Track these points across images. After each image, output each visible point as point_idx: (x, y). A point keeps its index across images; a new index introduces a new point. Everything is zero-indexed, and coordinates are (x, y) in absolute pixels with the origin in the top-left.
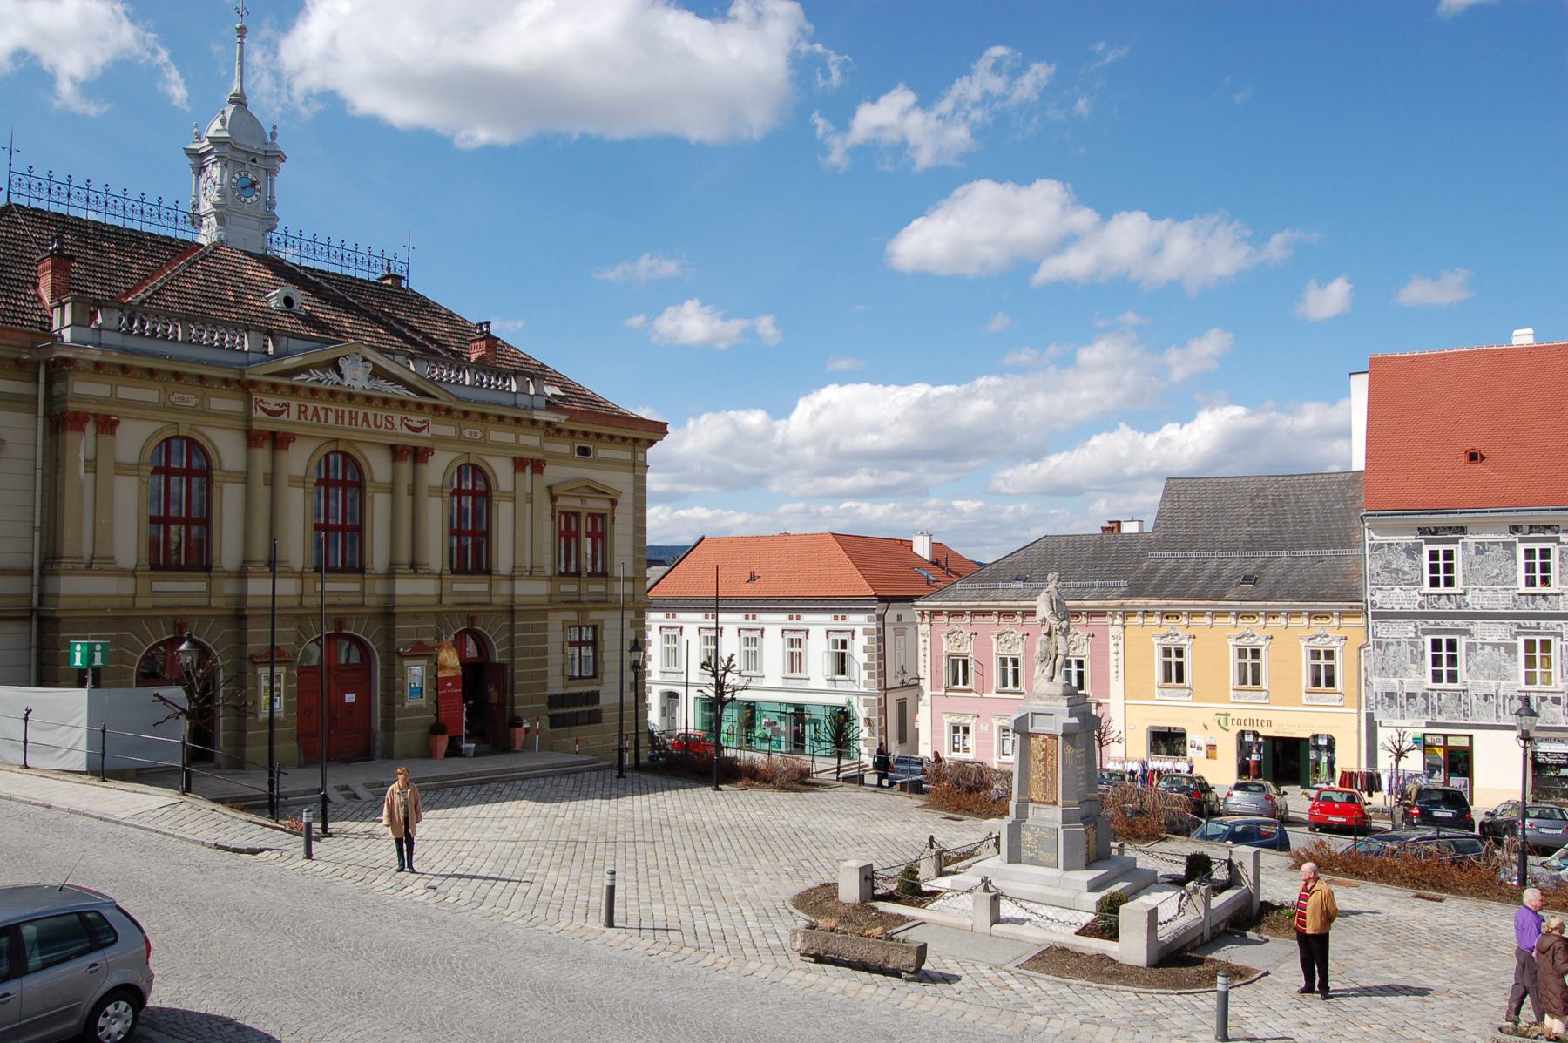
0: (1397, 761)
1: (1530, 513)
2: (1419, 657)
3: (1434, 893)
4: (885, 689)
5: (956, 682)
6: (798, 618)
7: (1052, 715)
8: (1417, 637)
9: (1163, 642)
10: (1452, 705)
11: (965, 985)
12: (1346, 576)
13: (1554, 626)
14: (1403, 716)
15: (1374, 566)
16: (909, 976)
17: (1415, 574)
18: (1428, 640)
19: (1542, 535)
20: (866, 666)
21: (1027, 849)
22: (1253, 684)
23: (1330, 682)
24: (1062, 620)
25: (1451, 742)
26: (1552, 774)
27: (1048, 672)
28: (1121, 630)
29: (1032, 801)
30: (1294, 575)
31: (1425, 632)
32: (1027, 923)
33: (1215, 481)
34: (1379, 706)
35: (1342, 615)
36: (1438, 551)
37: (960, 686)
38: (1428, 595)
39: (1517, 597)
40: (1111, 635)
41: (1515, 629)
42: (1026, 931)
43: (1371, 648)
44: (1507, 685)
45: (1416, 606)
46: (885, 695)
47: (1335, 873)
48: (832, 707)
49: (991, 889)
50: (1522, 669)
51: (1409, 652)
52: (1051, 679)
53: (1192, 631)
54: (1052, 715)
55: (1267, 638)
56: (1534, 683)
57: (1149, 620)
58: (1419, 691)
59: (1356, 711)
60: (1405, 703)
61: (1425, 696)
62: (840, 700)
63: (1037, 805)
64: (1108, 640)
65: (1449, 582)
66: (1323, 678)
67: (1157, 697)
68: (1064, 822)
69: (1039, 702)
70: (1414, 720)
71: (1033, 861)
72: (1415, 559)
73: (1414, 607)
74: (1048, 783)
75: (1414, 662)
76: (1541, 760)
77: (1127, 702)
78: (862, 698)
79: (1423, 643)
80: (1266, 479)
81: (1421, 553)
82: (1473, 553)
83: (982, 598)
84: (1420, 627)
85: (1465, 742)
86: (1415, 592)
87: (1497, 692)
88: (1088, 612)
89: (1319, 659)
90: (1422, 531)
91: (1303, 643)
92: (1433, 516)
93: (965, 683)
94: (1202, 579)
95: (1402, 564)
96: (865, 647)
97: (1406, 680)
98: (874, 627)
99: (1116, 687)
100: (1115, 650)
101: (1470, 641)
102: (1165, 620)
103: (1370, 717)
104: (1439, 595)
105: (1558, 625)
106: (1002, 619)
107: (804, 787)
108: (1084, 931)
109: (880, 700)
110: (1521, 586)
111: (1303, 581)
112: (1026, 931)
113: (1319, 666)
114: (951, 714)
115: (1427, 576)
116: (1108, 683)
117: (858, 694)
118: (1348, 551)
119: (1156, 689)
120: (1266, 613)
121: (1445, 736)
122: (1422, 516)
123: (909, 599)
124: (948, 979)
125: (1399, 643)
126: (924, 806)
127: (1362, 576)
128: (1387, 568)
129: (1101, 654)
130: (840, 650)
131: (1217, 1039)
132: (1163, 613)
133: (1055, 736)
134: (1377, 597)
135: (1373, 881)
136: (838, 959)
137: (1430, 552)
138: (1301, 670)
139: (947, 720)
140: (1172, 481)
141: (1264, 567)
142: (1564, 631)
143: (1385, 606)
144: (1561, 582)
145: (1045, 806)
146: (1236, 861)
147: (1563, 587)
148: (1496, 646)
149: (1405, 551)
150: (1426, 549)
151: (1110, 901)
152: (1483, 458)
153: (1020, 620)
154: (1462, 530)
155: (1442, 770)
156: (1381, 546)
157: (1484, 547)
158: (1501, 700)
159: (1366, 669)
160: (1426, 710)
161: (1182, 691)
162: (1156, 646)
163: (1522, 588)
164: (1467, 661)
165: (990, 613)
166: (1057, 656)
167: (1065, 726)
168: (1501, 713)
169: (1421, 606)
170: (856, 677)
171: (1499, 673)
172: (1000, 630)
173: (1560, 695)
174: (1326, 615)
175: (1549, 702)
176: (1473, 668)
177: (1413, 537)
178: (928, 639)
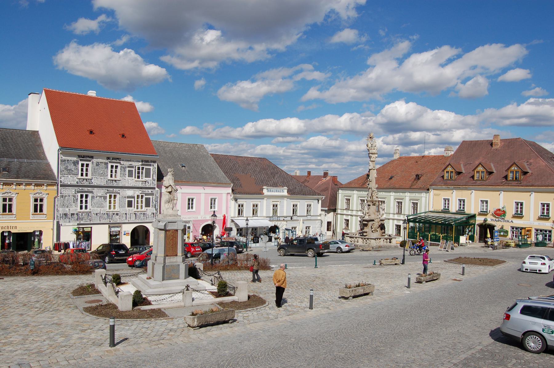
8: (76, 194)
10: (86, 217)
14: (69, 222)
17: (76, 171)
18: (79, 195)
19: (116, 161)
25: (86, 230)
26: (114, 238)
31: (78, 192)
34: (61, 219)
35: (48, 185)
38: (80, 179)
43: (59, 197)
44: (103, 210)
45: (76, 183)
59: (52, 221)
60: (70, 217)
61: (77, 214)
63: (169, 257)
66: (38, 208)
72: (76, 166)
73: (75, 183)
76: (112, 234)
84: (76, 190)
85: (89, 230)
90: (79, 156)
91: (31, 196)
95: (71, 167)
103: (58, 223)
104: (84, 179)
118: (41, 161)
121: (83, 228)
128: (66, 169)
133: (177, 230)
138: (30, 206)
148: (101, 197)
154: (92, 157)
156: (65, 160)
158: (101, 215)
159: (57, 205)
160: (78, 219)
163: (109, 178)
168: (101, 219)
169: (77, 183)
176: (93, 204)
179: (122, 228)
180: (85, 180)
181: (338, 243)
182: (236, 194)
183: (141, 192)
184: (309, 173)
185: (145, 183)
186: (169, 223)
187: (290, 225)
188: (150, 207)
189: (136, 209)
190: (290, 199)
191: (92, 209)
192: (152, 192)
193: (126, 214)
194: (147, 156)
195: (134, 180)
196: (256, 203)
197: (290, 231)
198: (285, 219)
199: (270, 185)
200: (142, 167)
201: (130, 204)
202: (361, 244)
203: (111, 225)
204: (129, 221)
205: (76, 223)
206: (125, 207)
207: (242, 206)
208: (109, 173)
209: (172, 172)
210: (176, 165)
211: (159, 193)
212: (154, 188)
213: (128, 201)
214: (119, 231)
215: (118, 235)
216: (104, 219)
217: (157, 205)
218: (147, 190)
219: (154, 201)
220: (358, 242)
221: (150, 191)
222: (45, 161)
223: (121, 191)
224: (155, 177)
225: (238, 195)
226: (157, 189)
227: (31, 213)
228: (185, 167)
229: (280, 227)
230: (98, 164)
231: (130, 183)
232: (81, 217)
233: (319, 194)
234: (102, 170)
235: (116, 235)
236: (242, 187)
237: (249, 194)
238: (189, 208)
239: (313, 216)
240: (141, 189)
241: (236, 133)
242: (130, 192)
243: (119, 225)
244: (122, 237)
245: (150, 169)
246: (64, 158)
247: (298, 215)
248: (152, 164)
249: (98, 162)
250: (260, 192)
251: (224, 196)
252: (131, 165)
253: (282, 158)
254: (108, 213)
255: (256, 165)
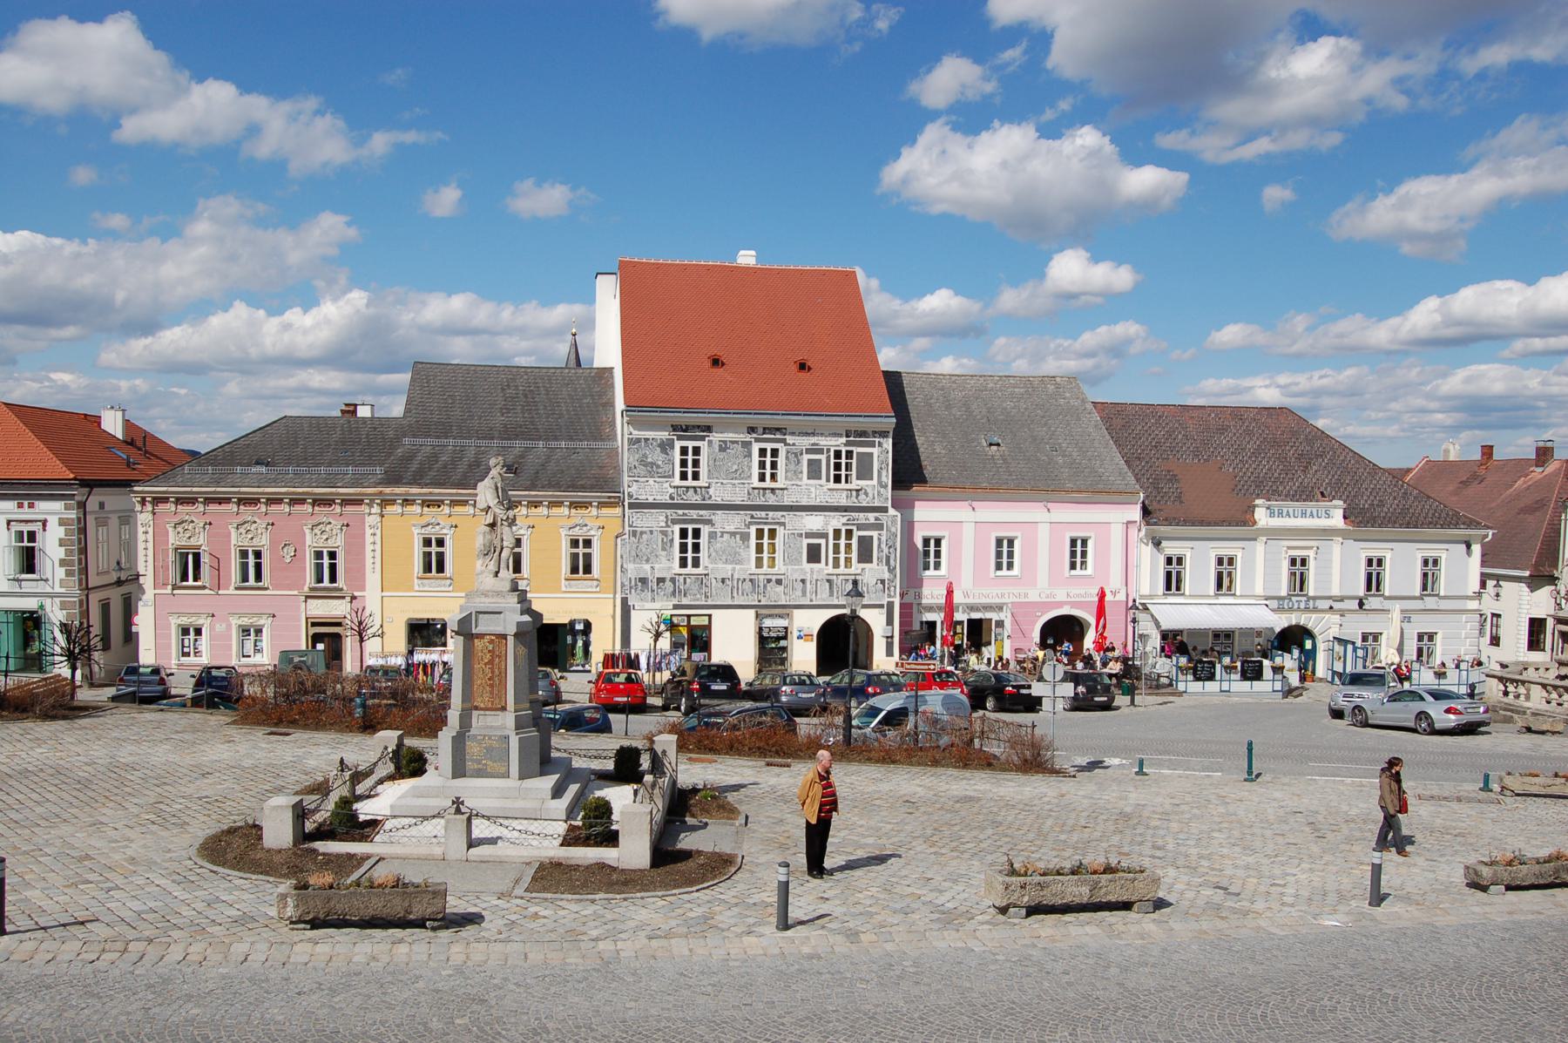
0: (656, 641)
1: (765, 416)
4: (87, 588)
5: (184, 577)
6: (31, 506)
7: (500, 613)
8: (668, 526)
10: (695, 588)
11: (491, 925)
14: (653, 600)
16: (436, 924)
17: (667, 468)
18: (677, 529)
19: (773, 436)
20: (63, 563)
21: (472, 760)
24: (508, 509)
25: (694, 621)
26: (773, 645)
27: (492, 567)
28: (379, 519)
29: (476, 708)
30: (552, 466)
31: (674, 522)
33: (464, 368)
34: (633, 591)
35: (601, 505)
36: (687, 447)
37: (191, 582)
38: (677, 487)
40: (139, 523)
42: (499, 850)
43: (627, 536)
44: (741, 569)
45: (668, 498)
46: (87, 596)
47: (690, 751)
48: (16, 612)
49: (463, 809)
53: (454, 521)
54: (500, 613)
57: (409, 508)
58: (668, 576)
59: (612, 596)
60: (655, 587)
61: (673, 580)
62: (30, 604)
63: (482, 712)
65: (696, 476)
66: (581, 566)
67: (416, 588)
69: (483, 599)
71: (480, 774)
72: (667, 454)
73: (666, 499)
74: (497, 682)
76: (765, 634)
77: (384, 594)
78: (57, 600)
80: (515, 370)
83: (218, 483)
84: (670, 517)
85: (705, 621)
86: (667, 485)
88: (343, 500)
90: (675, 428)
91: (563, 532)
92: (686, 415)
93: (195, 579)
95: (655, 458)
96: (60, 540)
98: (74, 516)
99: (373, 579)
102: (426, 509)
103: (624, 601)
104: (688, 488)
105: (783, 516)
106: (316, 508)
107: (71, 713)
109: (81, 602)
112: (499, 850)
113: (430, 553)
114: (180, 614)
116: (364, 574)
117: (52, 596)
118: (599, 444)
119: (416, 580)
120: (529, 502)
121: (689, 616)
122: (676, 414)
123: (127, 484)
124: (472, 919)
125: (651, 532)
126: (234, 722)
127: (617, 469)
128: (643, 461)
130: (26, 544)
131: (777, 928)
132: (424, 501)
133: (504, 637)
135: (725, 754)
138: (561, 558)
139: (175, 622)
141: (522, 457)
144: (786, 478)
146: (659, 749)
147: (788, 482)
148: (733, 534)
149: (659, 446)
152: (723, 364)
153: (263, 508)
154: (709, 429)
156: (638, 440)
158: (735, 582)
159: (622, 557)
160: (674, 593)
161: (443, 582)
163: (756, 482)
165: (228, 501)
166: (502, 549)
168: (735, 594)
169: (672, 498)
170: (49, 575)
171: (735, 559)
172: (240, 520)
176: (714, 554)
178: (151, 530)
179: (792, 619)
180: (691, 491)
181: (1422, 699)
182: (1155, 524)
183: (844, 520)
184: (1488, 451)
185: (858, 495)
186: (481, 616)
187: (1355, 627)
188: (872, 562)
189: (830, 569)
190: (1355, 540)
191: (710, 566)
192: (877, 519)
193: (803, 581)
194: (861, 419)
195: (825, 488)
196: (1230, 553)
197: (1350, 647)
198: (1337, 605)
199: (1286, 496)
200: (847, 452)
201: (814, 555)
202: (1540, 707)
203: (762, 612)
204: (811, 600)
205: (671, 603)
206: (799, 562)
207: (1180, 561)
208: (756, 471)
209: (499, 467)
210: (973, 440)
211: (899, 523)
212: (885, 510)
213: (808, 545)
214: (786, 628)
215: (785, 638)
216: (743, 594)
217: (892, 556)
218: (862, 515)
219: (883, 546)
220: (1528, 698)
221: (871, 517)
222: (608, 445)
223: (788, 517)
224: (887, 476)
225: (1162, 528)
226: (892, 512)
227: (563, 576)
228: (998, 445)
229: (1316, 631)
230: (724, 447)
231: (813, 496)
232: (682, 587)
233: (1471, 524)
234: (734, 463)
235: (778, 639)
236: (1181, 502)
237: (1202, 523)
238: (1073, 566)
239: (1445, 597)
240: (846, 511)
241: (1381, 334)
242: (814, 522)
243: (785, 610)
244: (792, 644)
245: (871, 454)
246: (637, 434)
247: (1387, 594)
248: (877, 440)
249: (725, 442)
250: (1244, 519)
251: (1117, 533)
252: (817, 445)
253: (1542, 404)
254: (752, 577)
255: (1249, 433)
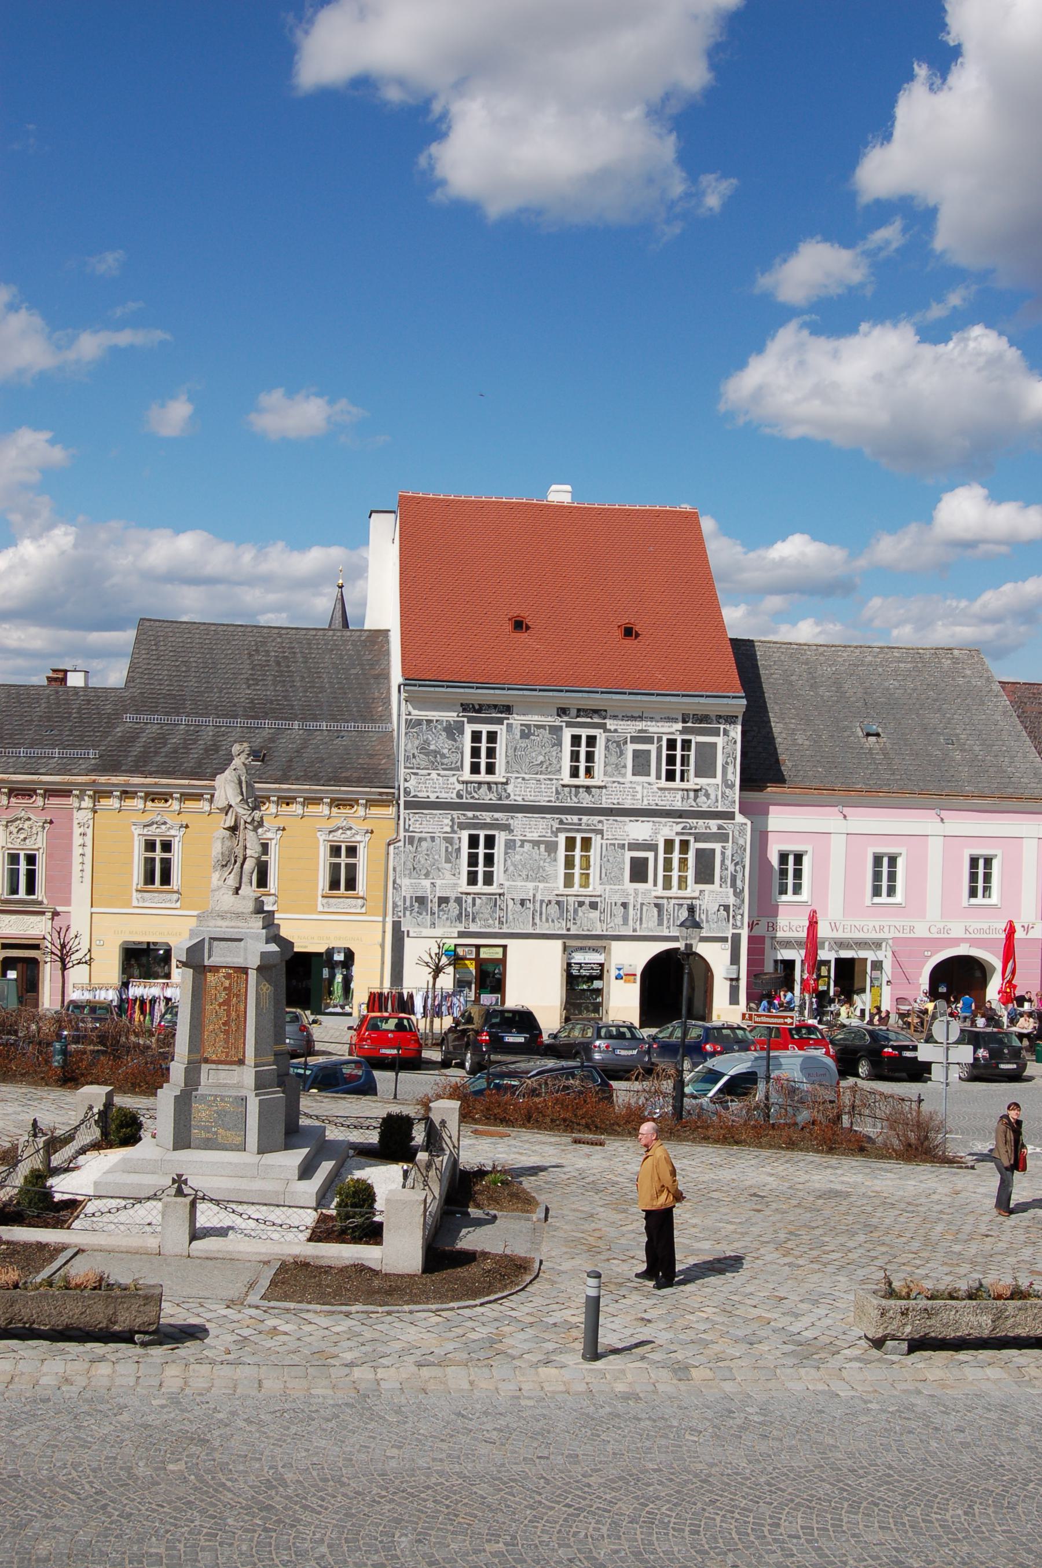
0: (435, 978)
2: (454, 855)
3: (591, 1136)
7: (240, 940)
8: (453, 832)
9: (145, 832)
10: (487, 911)
12: (371, 756)
13: (595, 822)
15: (410, 745)
16: (147, 1338)
17: (455, 758)
18: (465, 835)
19: (589, 720)
21: (198, 1127)
22: (347, 889)
23: (351, 885)
24: (253, 809)
25: (484, 954)
26: (585, 987)
27: (232, 881)
28: (90, 815)
29: (207, 1061)
31: (462, 826)
32: (231, 1232)
33: (202, 628)
34: (408, 913)
35: (370, 803)
36: (481, 732)
38: (467, 783)
39: (560, 789)
40: (75, 822)
41: (556, 825)
43: (401, 844)
45: (454, 796)
47: (476, 1121)
50: (561, 870)
51: (444, 849)
52: (237, 890)
53: (185, 819)
54: (240, 940)
55: (279, 829)
56: (670, 889)
57: (128, 803)
58: (452, 895)
59: (381, 919)
60: (436, 909)
63: (214, 1066)
64: (71, 828)
65: (491, 769)
67: (135, 903)
68: (257, 1087)
69: (220, 923)
70: (446, 930)
71: (209, 1145)
72: (455, 740)
73: (452, 797)
75: (448, 861)
76: (575, 972)
77: (94, 910)
79: (460, 838)
81: (463, 733)
82: (518, 737)
84: (456, 821)
85: (498, 953)
86: (454, 779)
87: (534, 896)
89: (154, 850)
90: (465, 707)
91: (322, 837)
94: (196, 752)
95: (440, 744)
97: (438, 882)
99: (80, 890)
100: (81, 842)
101: (510, 837)
103: (397, 925)
104: (480, 783)
105: (600, 822)
108: (321, 1233)
110: (566, 778)
111: (322, 760)
115: (468, 760)
118: (369, 726)
119: (135, 894)
121: (478, 947)
124: (193, 1333)
125: (433, 839)
127: (392, 759)
128: (424, 749)
129: (61, 850)
132: (147, 794)
133: (244, 970)
134: (412, 784)
135: (520, 1127)
136: (31, 1329)
137: (473, 732)
140: (148, 624)
141: (272, 740)
142: (605, 828)
143: (420, 795)
145: (227, 1067)
146: (436, 1119)
148: (536, 844)
150: (469, 729)
151: (355, 1192)
152: (528, 628)
154: (508, 709)
155: (473, 986)
156: (419, 723)
157: (530, 730)
158: (538, 905)
159: (394, 869)
160: (459, 918)
161: (168, 896)
162: (136, 838)
163: (567, 779)
164: (505, 860)
166: (245, 859)
167: (263, 955)
168: (537, 920)
171: (538, 875)
173: (598, 899)
174: (350, 803)
175: (586, 907)
176: (511, 869)
177: (455, 714)
